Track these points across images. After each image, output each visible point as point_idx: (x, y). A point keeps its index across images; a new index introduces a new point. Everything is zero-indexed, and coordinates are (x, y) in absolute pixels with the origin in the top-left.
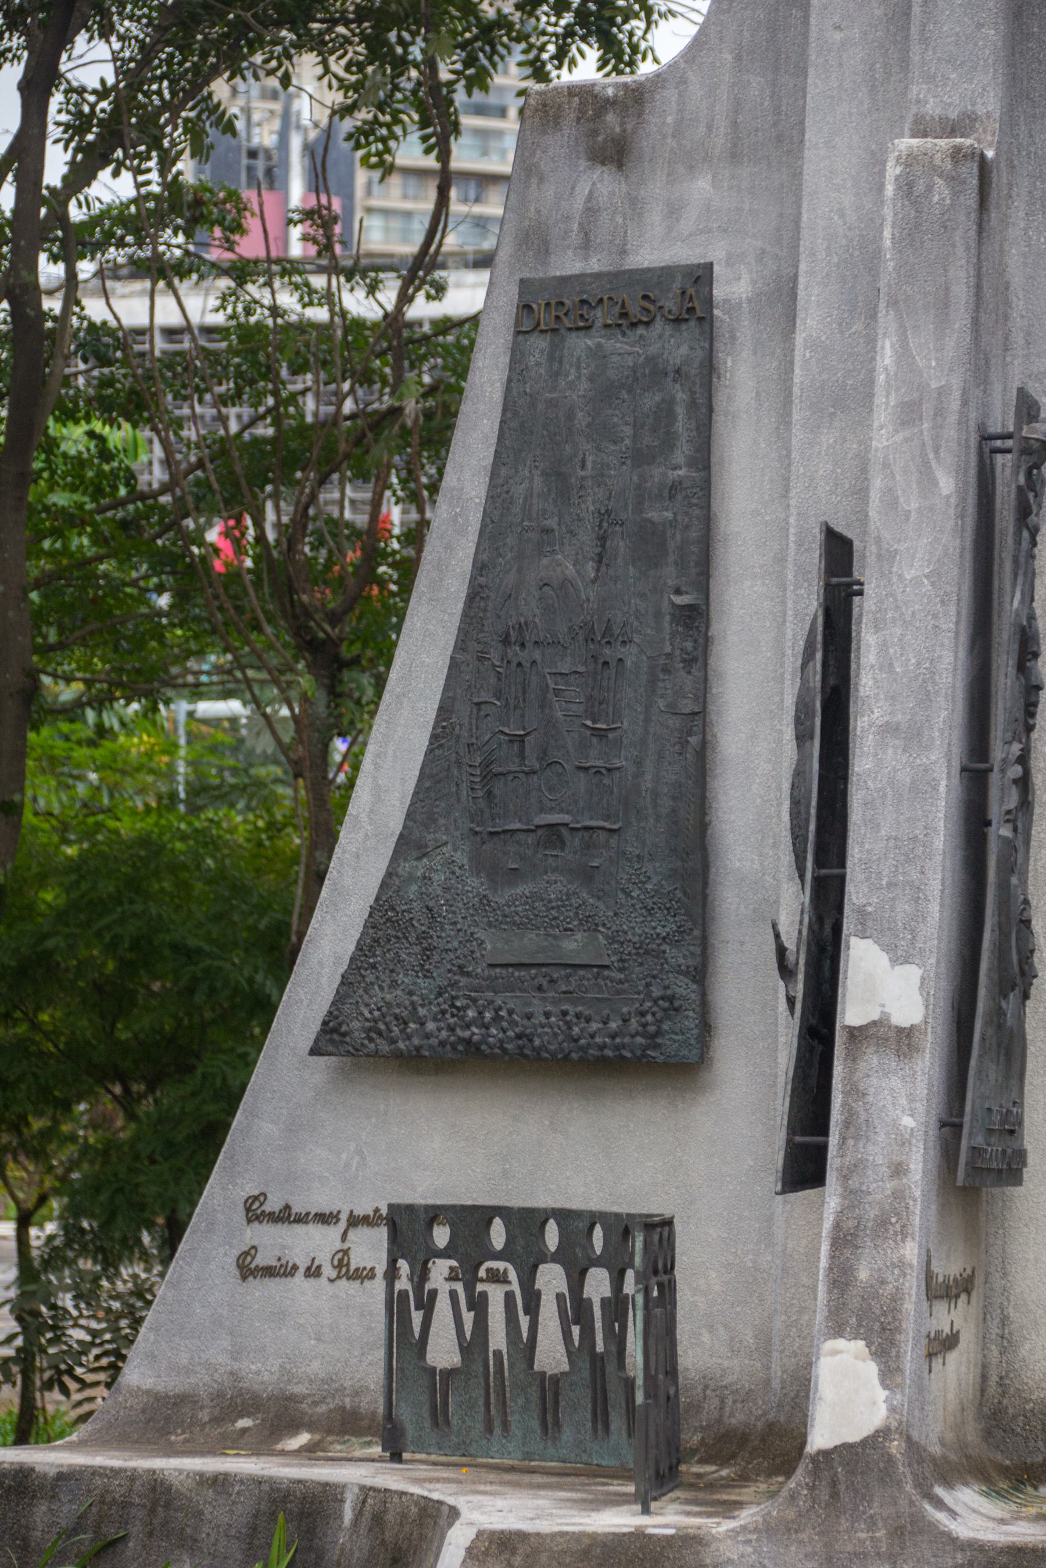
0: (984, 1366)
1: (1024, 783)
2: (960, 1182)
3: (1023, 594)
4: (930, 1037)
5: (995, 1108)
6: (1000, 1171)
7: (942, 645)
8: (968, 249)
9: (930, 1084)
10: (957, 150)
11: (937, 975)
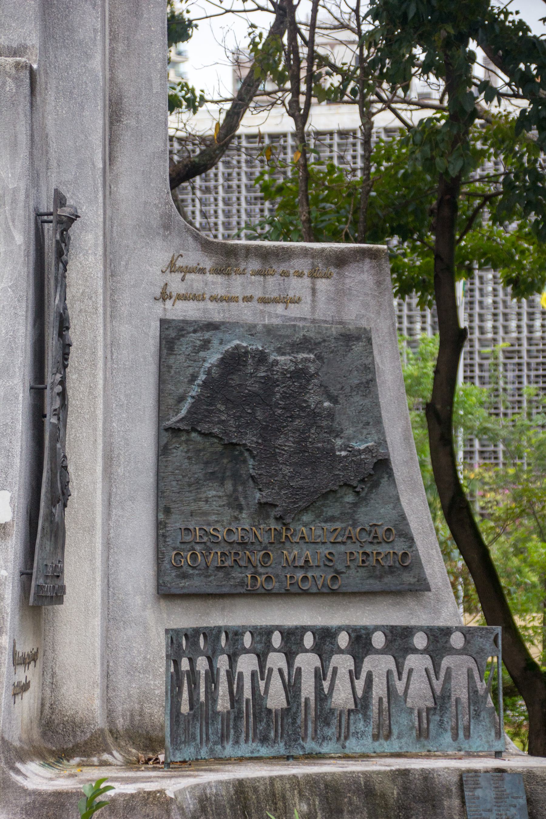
0: (43, 699)
1: (63, 395)
2: (31, 604)
3: (60, 296)
4: (15, 529)
5: (49, 564)
6: (52, 597)
7: (19, 323)
8: (26, 115)
9: (16, 553)
10: (17, 64)
11: (19, 495)
